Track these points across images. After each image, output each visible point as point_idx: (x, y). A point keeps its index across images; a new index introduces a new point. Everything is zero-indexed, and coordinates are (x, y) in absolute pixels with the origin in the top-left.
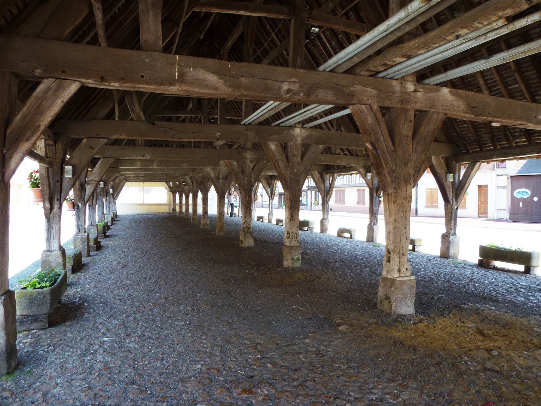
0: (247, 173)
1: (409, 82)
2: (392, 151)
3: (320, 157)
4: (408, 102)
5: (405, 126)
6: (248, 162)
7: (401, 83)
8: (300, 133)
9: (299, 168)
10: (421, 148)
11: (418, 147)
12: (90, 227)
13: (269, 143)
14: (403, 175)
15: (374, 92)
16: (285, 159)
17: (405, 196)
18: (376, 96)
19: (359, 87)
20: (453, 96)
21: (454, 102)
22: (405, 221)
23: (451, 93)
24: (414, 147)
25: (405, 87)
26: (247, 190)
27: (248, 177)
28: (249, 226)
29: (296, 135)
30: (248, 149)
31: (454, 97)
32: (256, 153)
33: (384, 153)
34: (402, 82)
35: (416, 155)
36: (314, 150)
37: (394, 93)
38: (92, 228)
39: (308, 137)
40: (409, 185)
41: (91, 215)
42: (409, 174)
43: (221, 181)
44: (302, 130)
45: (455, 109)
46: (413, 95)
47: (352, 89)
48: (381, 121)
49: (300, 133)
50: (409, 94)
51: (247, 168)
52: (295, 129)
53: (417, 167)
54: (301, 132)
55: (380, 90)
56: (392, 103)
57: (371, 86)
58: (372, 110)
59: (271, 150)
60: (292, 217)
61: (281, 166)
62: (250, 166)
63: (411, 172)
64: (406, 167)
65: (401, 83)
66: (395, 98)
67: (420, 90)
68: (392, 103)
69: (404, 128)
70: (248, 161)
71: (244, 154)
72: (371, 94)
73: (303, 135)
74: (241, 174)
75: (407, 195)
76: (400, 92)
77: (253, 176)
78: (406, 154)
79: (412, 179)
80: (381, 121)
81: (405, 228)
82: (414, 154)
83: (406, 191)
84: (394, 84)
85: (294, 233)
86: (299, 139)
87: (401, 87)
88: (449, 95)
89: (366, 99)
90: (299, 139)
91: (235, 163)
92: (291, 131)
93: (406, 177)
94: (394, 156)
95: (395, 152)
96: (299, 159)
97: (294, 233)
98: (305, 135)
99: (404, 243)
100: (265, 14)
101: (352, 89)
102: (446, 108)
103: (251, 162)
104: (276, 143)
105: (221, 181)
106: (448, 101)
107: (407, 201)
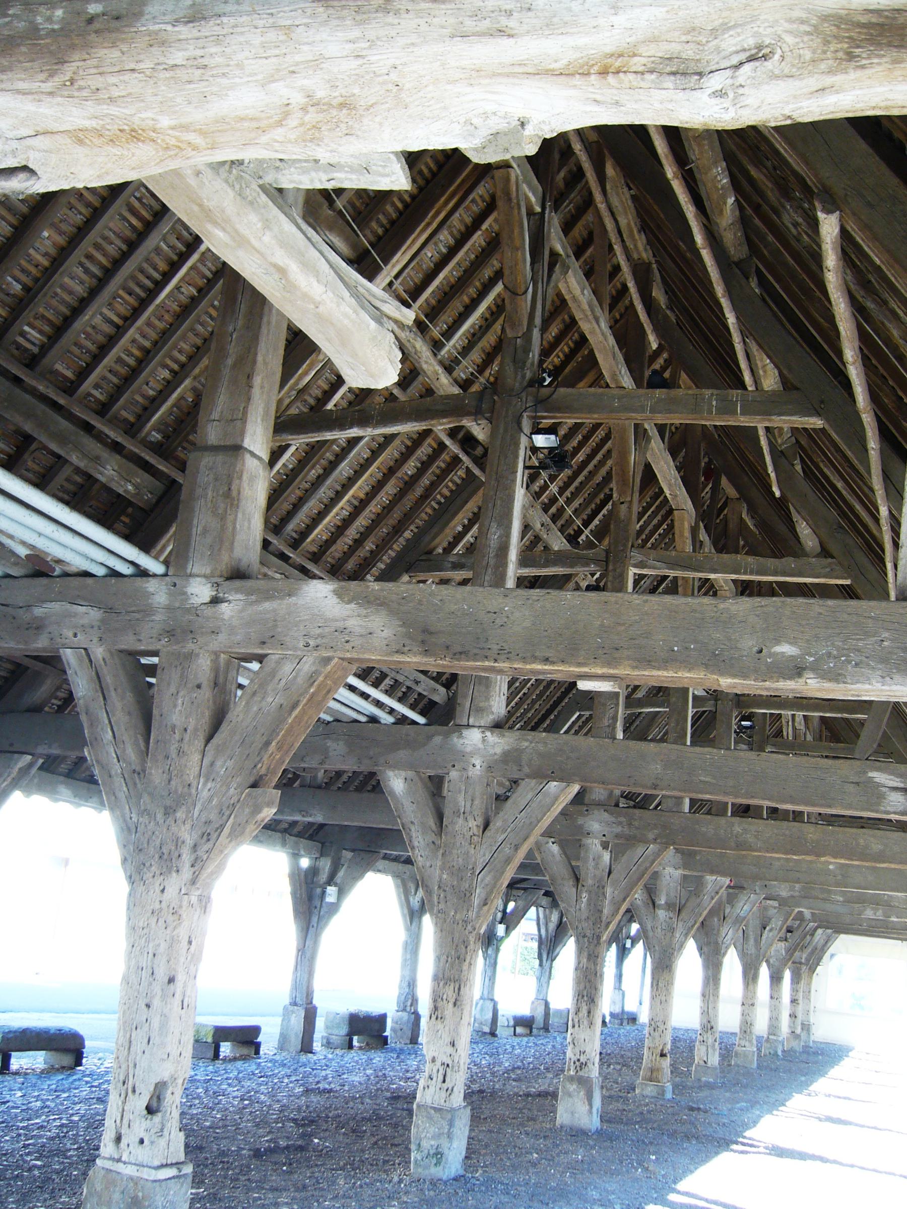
0: (590, 882)
1: (198, 579)
2: (134, 771)
3: (862, 841)
4: (190, 632)
5: (180, 702)
6: (594, 845)
7: (175, 585)
8: (481, 746)
9: (472, 851)
10: (229, 763)
11: (219, 763)
12: (291, 1008)
13: (390, 773)
14: (158, 843)
15: (94, 615)
16: (431, 822)
17: (157, 906)
18: (96, 624)
19: (56, 607)
20: (349, 602)
21: (354, 623)
22: (150, 984)
23: (338, 594)
24: (206, 761)
25: (185, 593)
26: (584, 936)
27: (590, 892)
28: (583, 1059)
29: (469, 749)
30: (599, 804)
31: (353, 606)
32: (622, 819)
33: (110, 776)
34: (176, 580)
35: (209, 785)
36: (529, 796)
37: (147, 611)
38: (293, 1012)
39: (509, 757)
40: (174, 874)
41: (299, 974)
42: (178, 843)
43: (662, 914)
44: (488, 734)
45: (356, 642)
46: (209, 611)
47: (38, 611)
48: (112, 689)
49: (481, 746)
50: (195, 611)
51: (591, 864)
52: (466, 732)
53: (208, 822)
54: (484, 740)
55: (110, 610)
56: (140, 640)
57: (85, 600)
58: (91, 661)
59: (392, 793)
60: (436, 1008)
61: (416, 844)
62: (599, 857)
63: (188, 836)
64: (170, 820)
65: (175, 585)
66: (151, 624)
67: (231, 598)
68: (140, 640)
69: (175, 706)
70: (596, 841)
71: (580, 821)
72: (85, 621)
73: (492, 751)
74: (571, 882)
75: (164, 905)
76: (169, 608)
77: (609, 891)
78: (173, 783)
79: (187, 857)
80: (112, 689)
81: (148, 1006)
82: (205, 784)
83: (163, 891)
84: (151, 590)
85: (438, 1063)
86: (478, 762)
87: (170, 594)
88: (333, 600)
89: (71, 634)
90: (478, 762)
91: (555, 848)
92: (455, 740)
93: (165, 850)
94: (139, 786)
95: (140, 773)
96: (474, 824)
97: (438, 1063)
98: (498, 750)
99: (139, 1052)
100: (415, 424)
101: (38, 611)
102: (319, 641)
103: (605, 846)
104: (410, 774)
105: (662, 914)
106: (326, 620)
107: (161, 921)
